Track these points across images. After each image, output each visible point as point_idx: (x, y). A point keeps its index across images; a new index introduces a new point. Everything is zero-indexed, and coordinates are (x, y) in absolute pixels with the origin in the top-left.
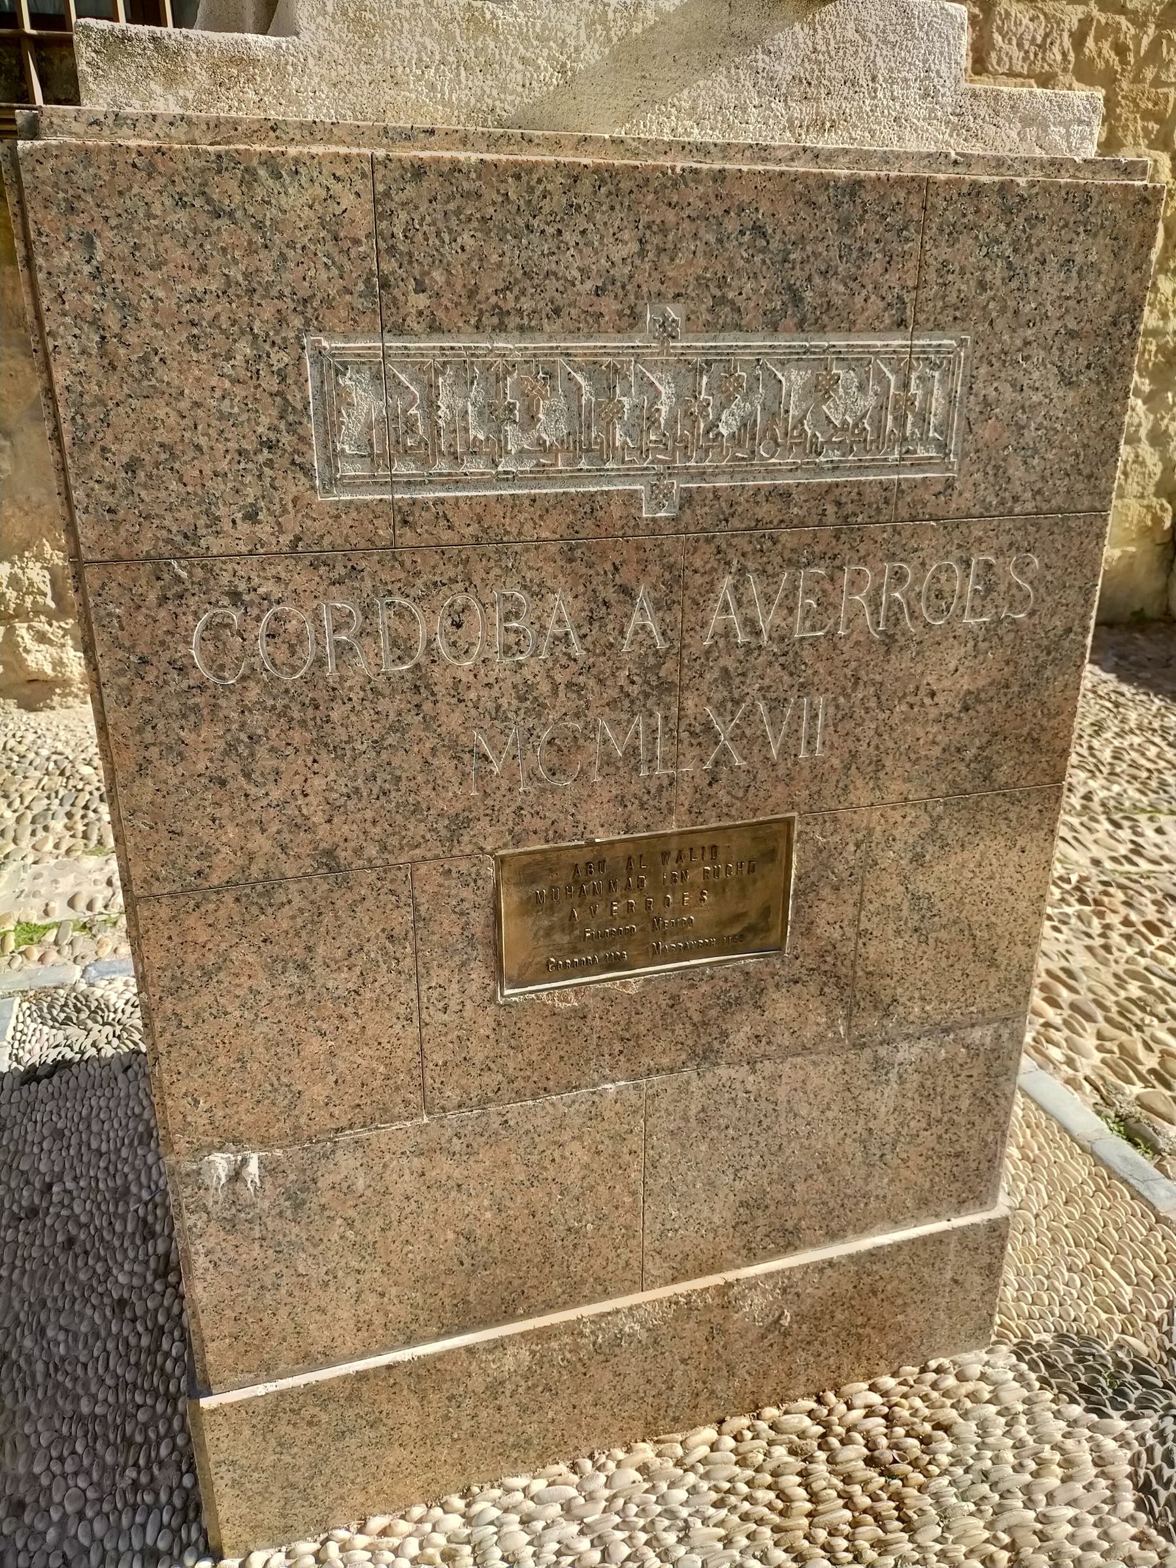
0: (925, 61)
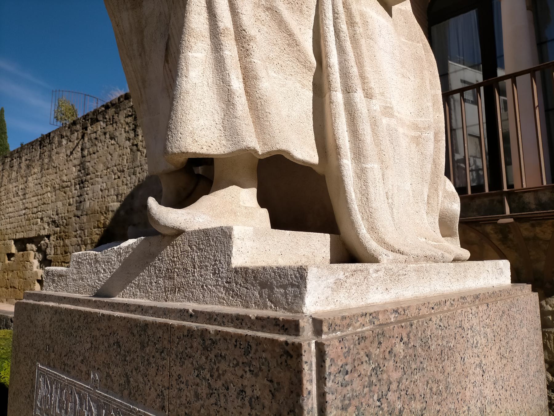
0: (214, 256)
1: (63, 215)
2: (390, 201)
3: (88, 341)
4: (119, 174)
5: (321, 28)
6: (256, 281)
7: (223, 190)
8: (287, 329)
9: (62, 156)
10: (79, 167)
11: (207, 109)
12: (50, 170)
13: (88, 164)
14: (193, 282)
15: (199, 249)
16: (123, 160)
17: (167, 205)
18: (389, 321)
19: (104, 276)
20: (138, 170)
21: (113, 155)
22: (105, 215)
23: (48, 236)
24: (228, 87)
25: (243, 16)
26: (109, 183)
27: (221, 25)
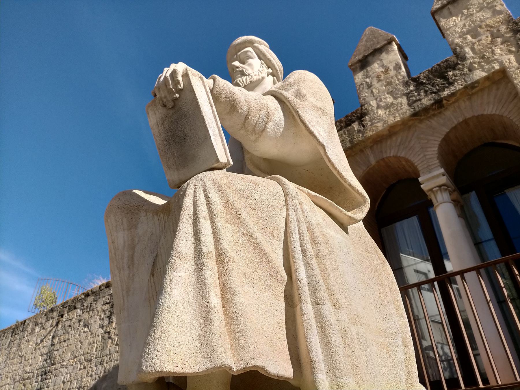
4: (86, 363)
5: (290, 247)
10: (45, 356)
12: (16, 359)
13: (56, 352)
16: (92, 348)
20: (106, 359)
21: (84, 343)
24: (207, 304)
26: (73, 374)
27: (205, 249)
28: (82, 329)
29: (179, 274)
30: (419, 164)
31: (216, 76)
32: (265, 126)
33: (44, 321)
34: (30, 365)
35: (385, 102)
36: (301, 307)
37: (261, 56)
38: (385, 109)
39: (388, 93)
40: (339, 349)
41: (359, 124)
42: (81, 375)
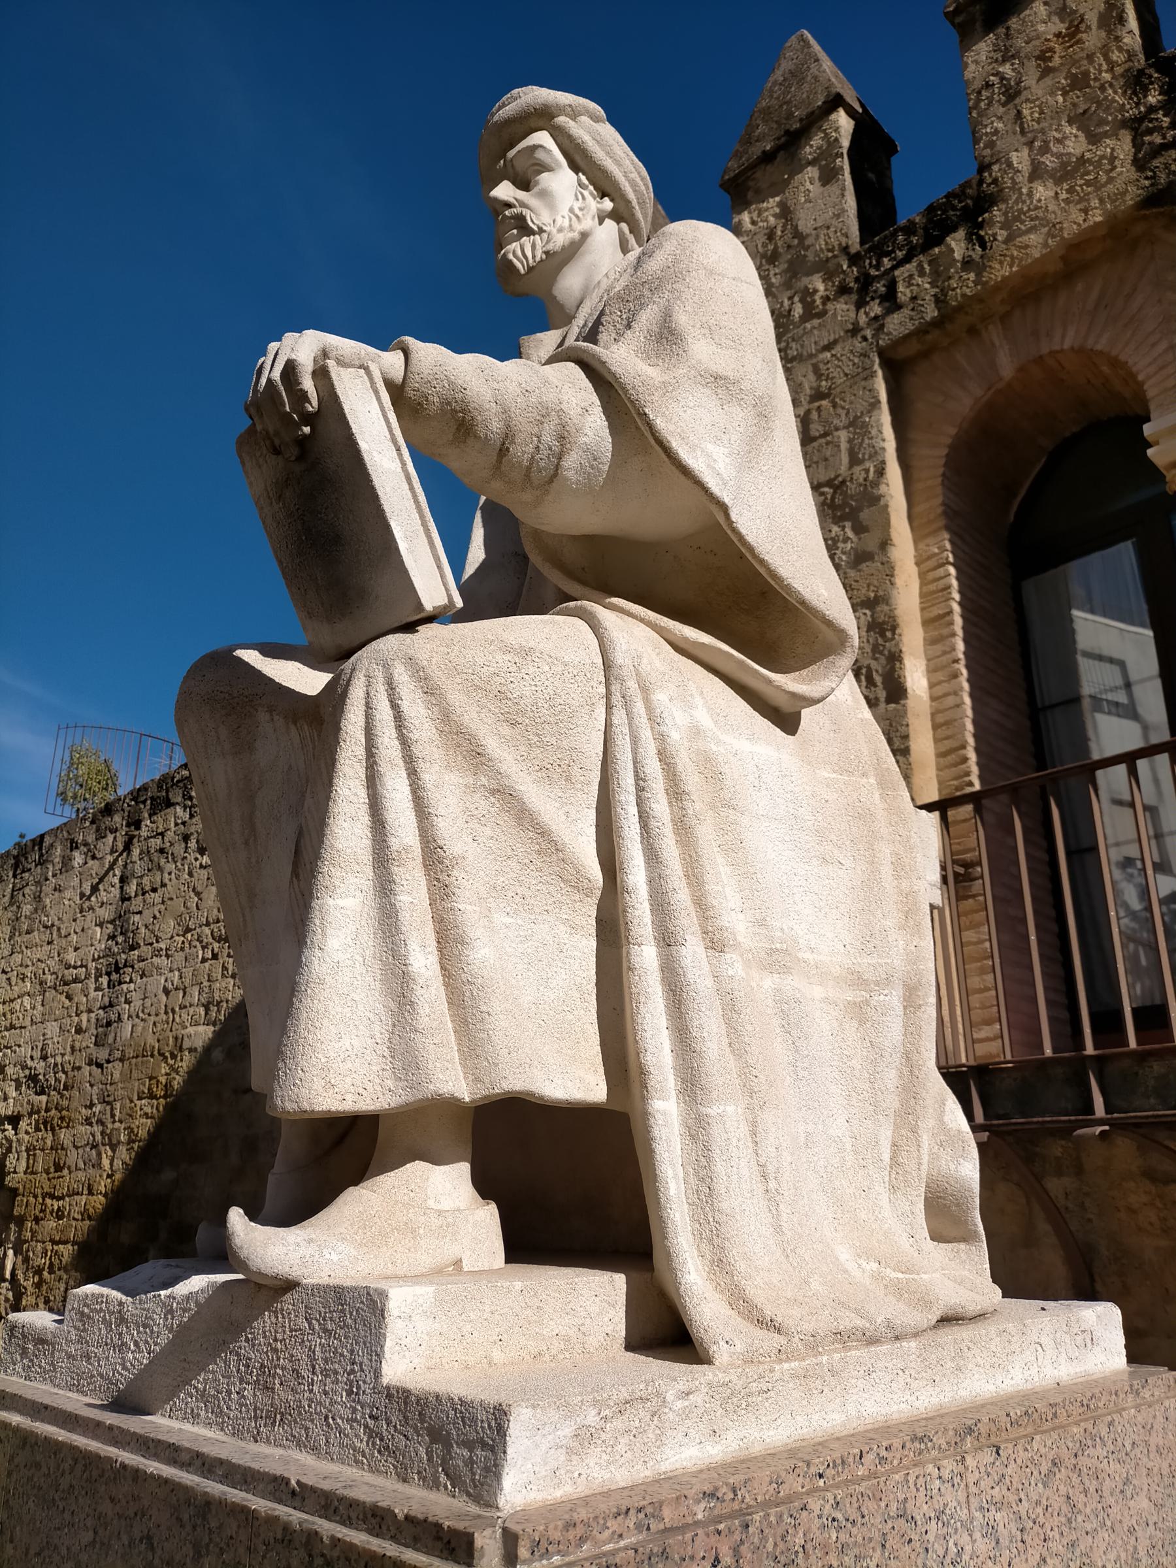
0: (352, 1352)
1: (59, 1059)
2: (772, 1185)
3: (89, 1524)
4: (216, 945)
6: (422, 1421)
7: (392, 1174)
8: (454, 1549)
9: (71, 896)
11: (359, 1013)
12: (36, 933)
13: (137, 918)
14: (309, 1406)
15: (325, 1330)
17: (264, 1223)
18: (689, 1520)
19: (135, 1358)
22: (171, 1062)
23: (14, 1120)
25: (440, 818)
26: (188, 972)
27: (394, 843)
28: (196, 859)
29: (340, 902)
30: (1149, 377)
31: (410, 341)
32: (557, 467)
33: (91, 839)
34: (76, 949)
35: (1059, 156)
36: (628, 952)
37: (578, 159)
38: (1058, 182)
39: (1070, 122)
40: (709, 1044)
41: (969, 239)
42: (209, 975)
